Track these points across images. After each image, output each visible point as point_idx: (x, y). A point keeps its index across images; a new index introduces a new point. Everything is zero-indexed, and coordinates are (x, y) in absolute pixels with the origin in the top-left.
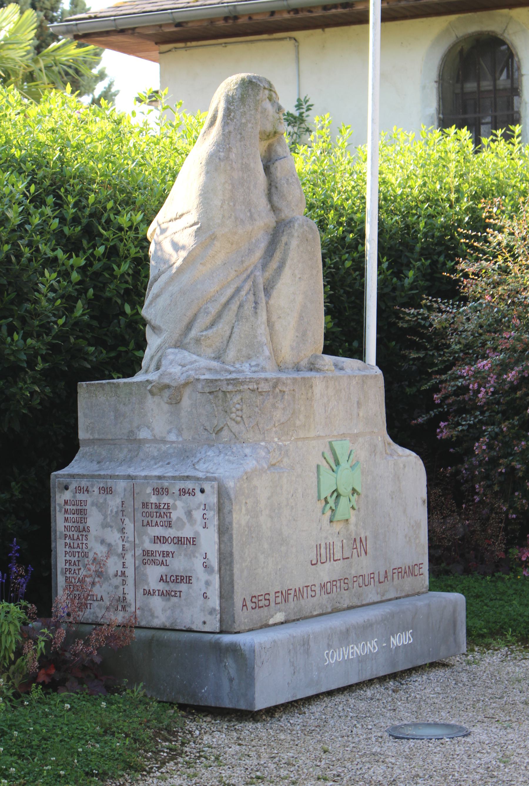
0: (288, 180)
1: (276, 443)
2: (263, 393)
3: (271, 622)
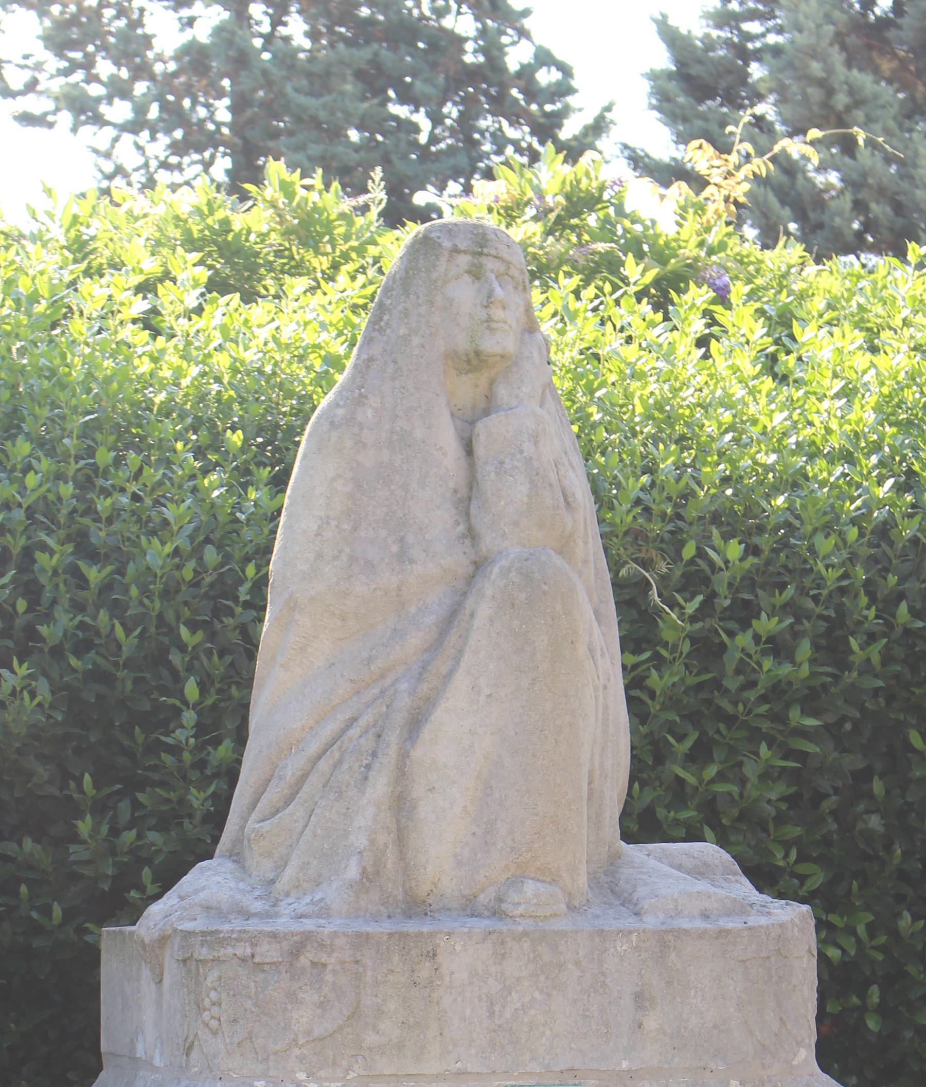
0: (502, 463)
2: (266, 968)
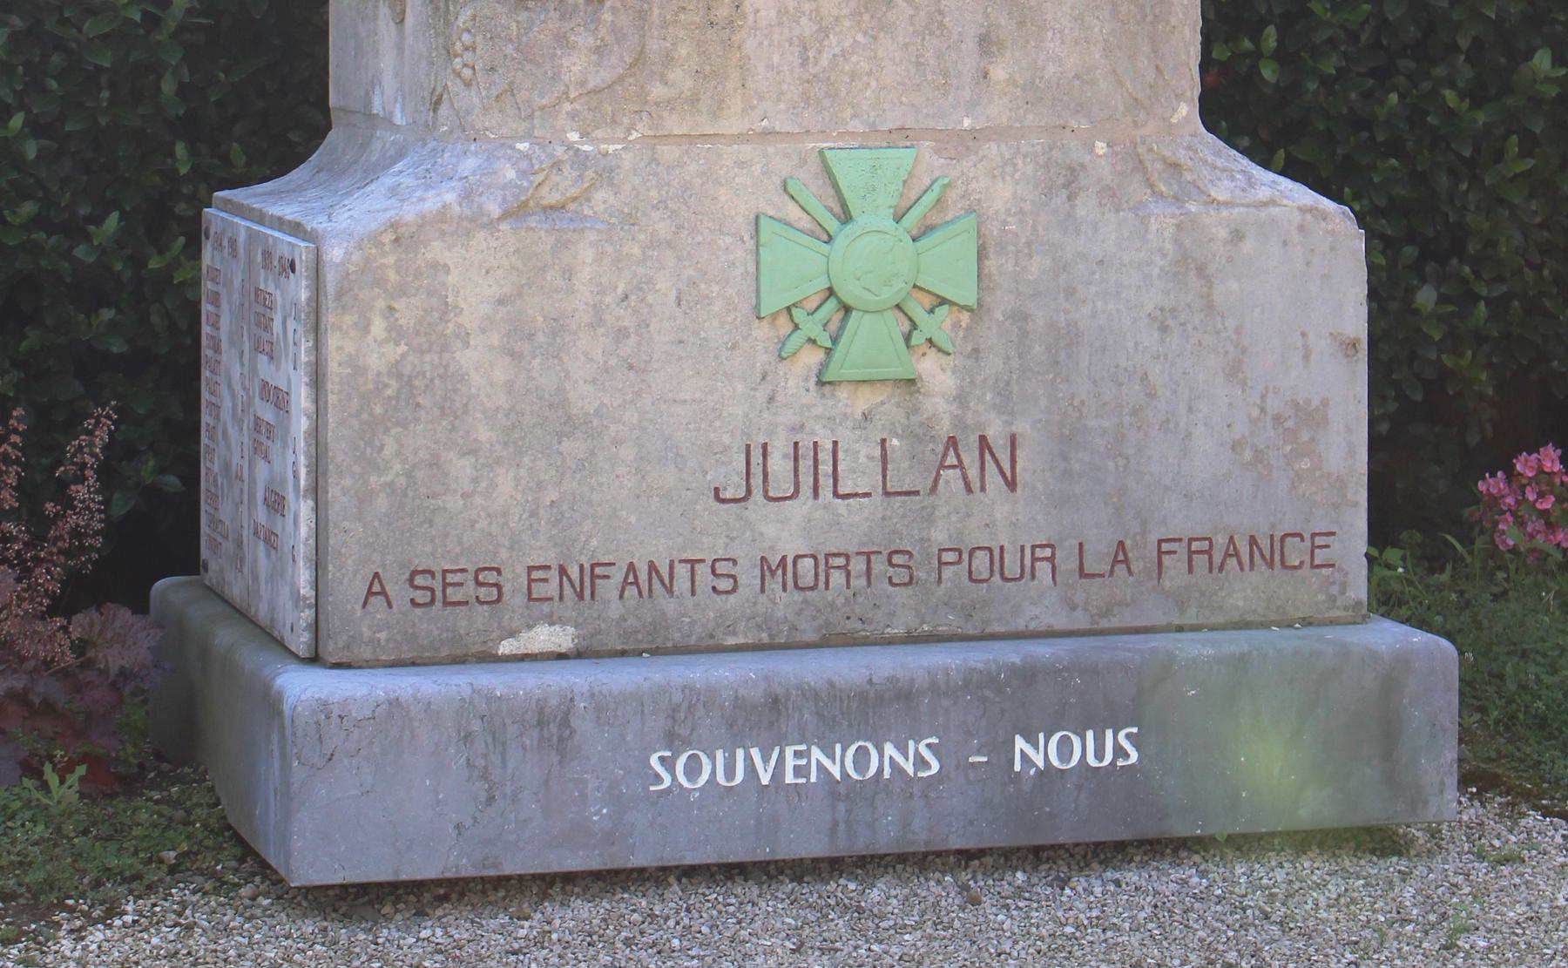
1: (569, 146)
3: (506, 647)
